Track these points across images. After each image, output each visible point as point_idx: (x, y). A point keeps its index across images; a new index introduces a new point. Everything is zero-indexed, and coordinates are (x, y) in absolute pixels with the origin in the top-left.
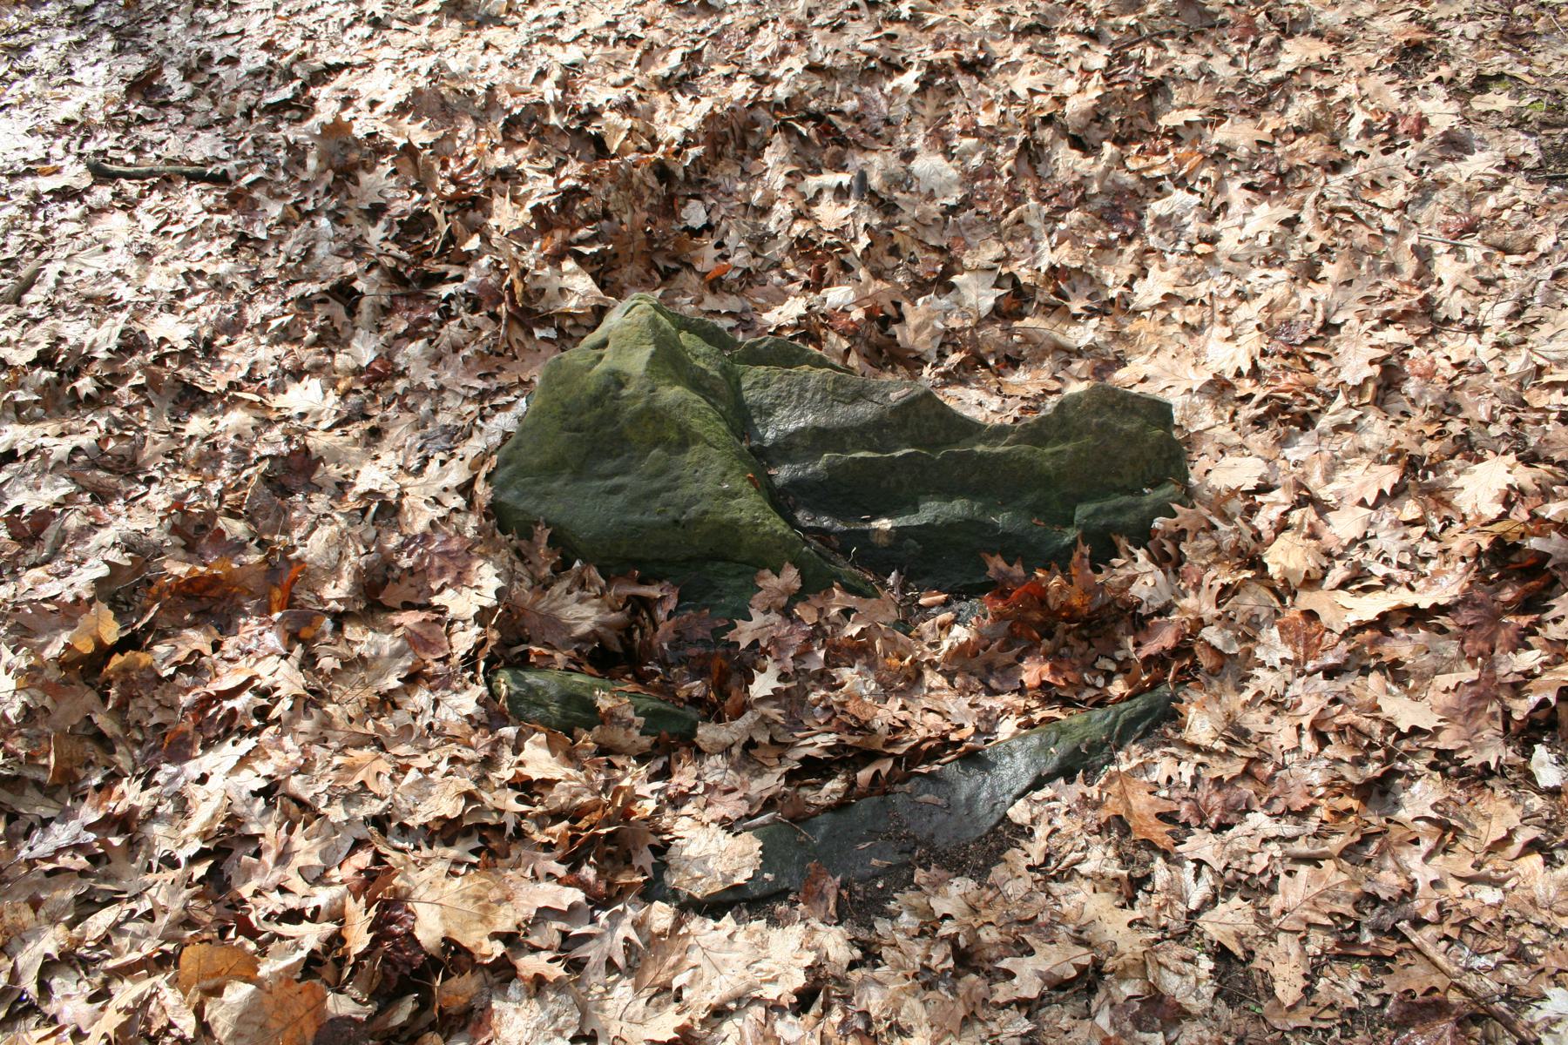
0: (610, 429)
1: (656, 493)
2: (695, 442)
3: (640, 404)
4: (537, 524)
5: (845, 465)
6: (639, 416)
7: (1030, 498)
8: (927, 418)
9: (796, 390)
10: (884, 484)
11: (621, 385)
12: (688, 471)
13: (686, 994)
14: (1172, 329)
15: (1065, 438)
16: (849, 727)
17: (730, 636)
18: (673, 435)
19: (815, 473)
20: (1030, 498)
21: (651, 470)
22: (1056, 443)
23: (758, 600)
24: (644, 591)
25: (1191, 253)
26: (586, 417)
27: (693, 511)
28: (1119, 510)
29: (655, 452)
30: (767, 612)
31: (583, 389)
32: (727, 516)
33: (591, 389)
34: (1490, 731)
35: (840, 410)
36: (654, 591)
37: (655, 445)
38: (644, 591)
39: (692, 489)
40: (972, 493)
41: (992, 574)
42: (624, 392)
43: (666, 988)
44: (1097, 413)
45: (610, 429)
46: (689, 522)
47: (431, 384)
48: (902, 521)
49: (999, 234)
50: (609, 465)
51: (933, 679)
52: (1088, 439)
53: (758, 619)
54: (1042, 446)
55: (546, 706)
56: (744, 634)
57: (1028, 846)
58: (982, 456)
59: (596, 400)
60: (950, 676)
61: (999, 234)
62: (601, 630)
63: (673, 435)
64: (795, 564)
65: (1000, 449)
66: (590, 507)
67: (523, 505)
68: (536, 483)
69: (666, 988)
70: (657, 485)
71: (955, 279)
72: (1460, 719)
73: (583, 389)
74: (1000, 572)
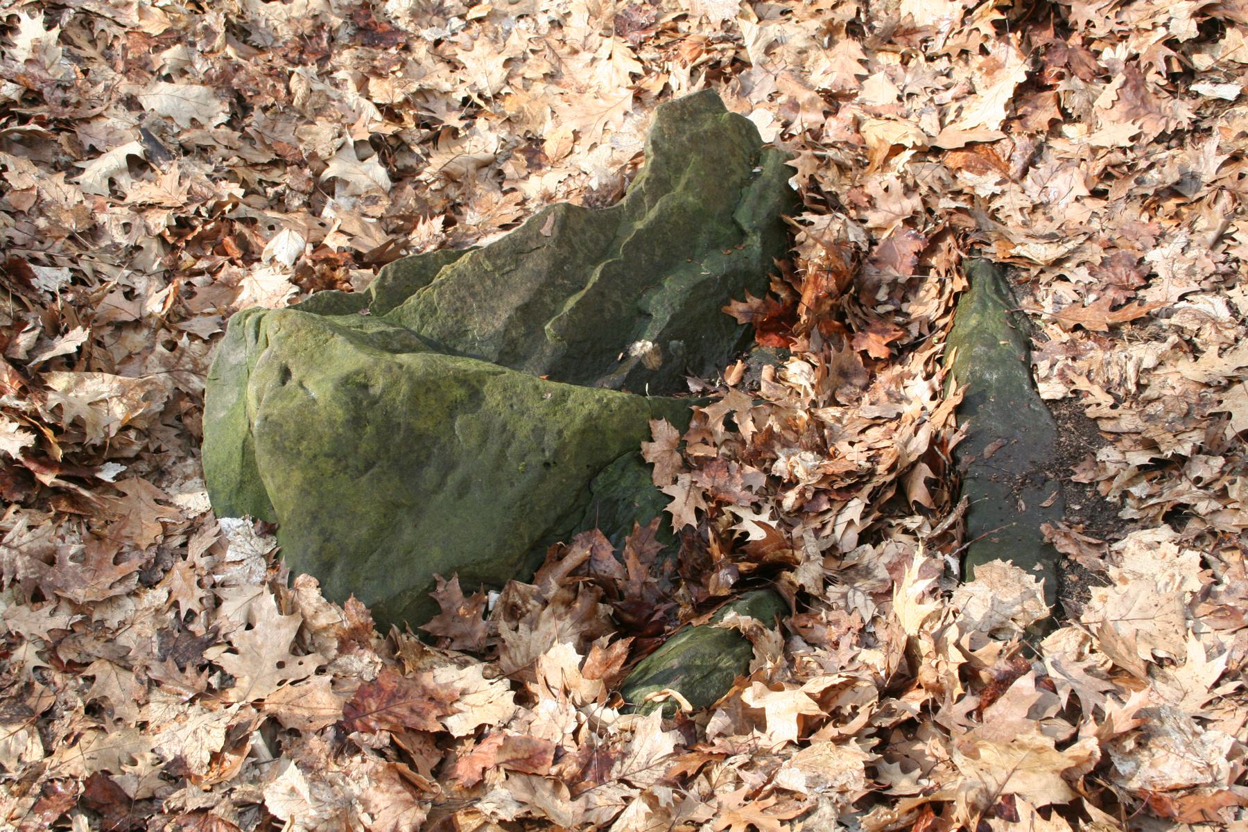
0: (398, 439)
1: (502, 455)
2: (482, 382)
3: (404, 388)
4: (435, 584)
5: (564, 323)
6: (413, 399)
7: (703, 239)
8: (583, 231)
9: (463, 293)
10: (607, 315)
11: (365, 387)
12: (505, 412)
13: (1161, 654)
14: (539, 88)
15: (679, 170)
16: (849, 488)
17: (677, 527)
18: (459, 393)
19: (555, 350)
20: (703, 239)
21: (473, 442)
22: (678, 179)
23: (660, 477)
24: (569, 562)
25: (468, 26)
26: (364, 447)
27: (550, 441)
28: (762, 197)
29: (457, 424)
30: (675, 481)
31: (332, 423)
32: (578, 420)
33: (340, 414)
34: (1167, 103)
35: (516, 278)
36: (577, 554)
37: (451, 416)
38: (569, 562)
39: (524, 428)
40: (666, 267)
41: (742, 320)
42: (376, 390)
43: (1149, 665)
44: (680, 132)
45: (398, 439)
46: (556, 453)
47: (63, 620)
48: (654, 329)
49: (302, 117)
50: (430, 473)
51: (828, 414)
52: (694, 158)
53: (678, 492)
54: (672, 188)
55: (716, 669)
56: (683, 511)
57: (1090, 400)
58: (650, 229)
59: (357, 422)
60: (833, 402)
61: (302, 117)
62: (585, 627)
63: (459, 393)
64: (657, 416)
65: (652, 215)
66: (452, 530)
67: (396, 586)
68: (387, 552)
69: (1149, 665)
70: (493, 448)
71: (328, 174)
72: (1142, 111)
73: (332, 423)
74: (745, 313)
